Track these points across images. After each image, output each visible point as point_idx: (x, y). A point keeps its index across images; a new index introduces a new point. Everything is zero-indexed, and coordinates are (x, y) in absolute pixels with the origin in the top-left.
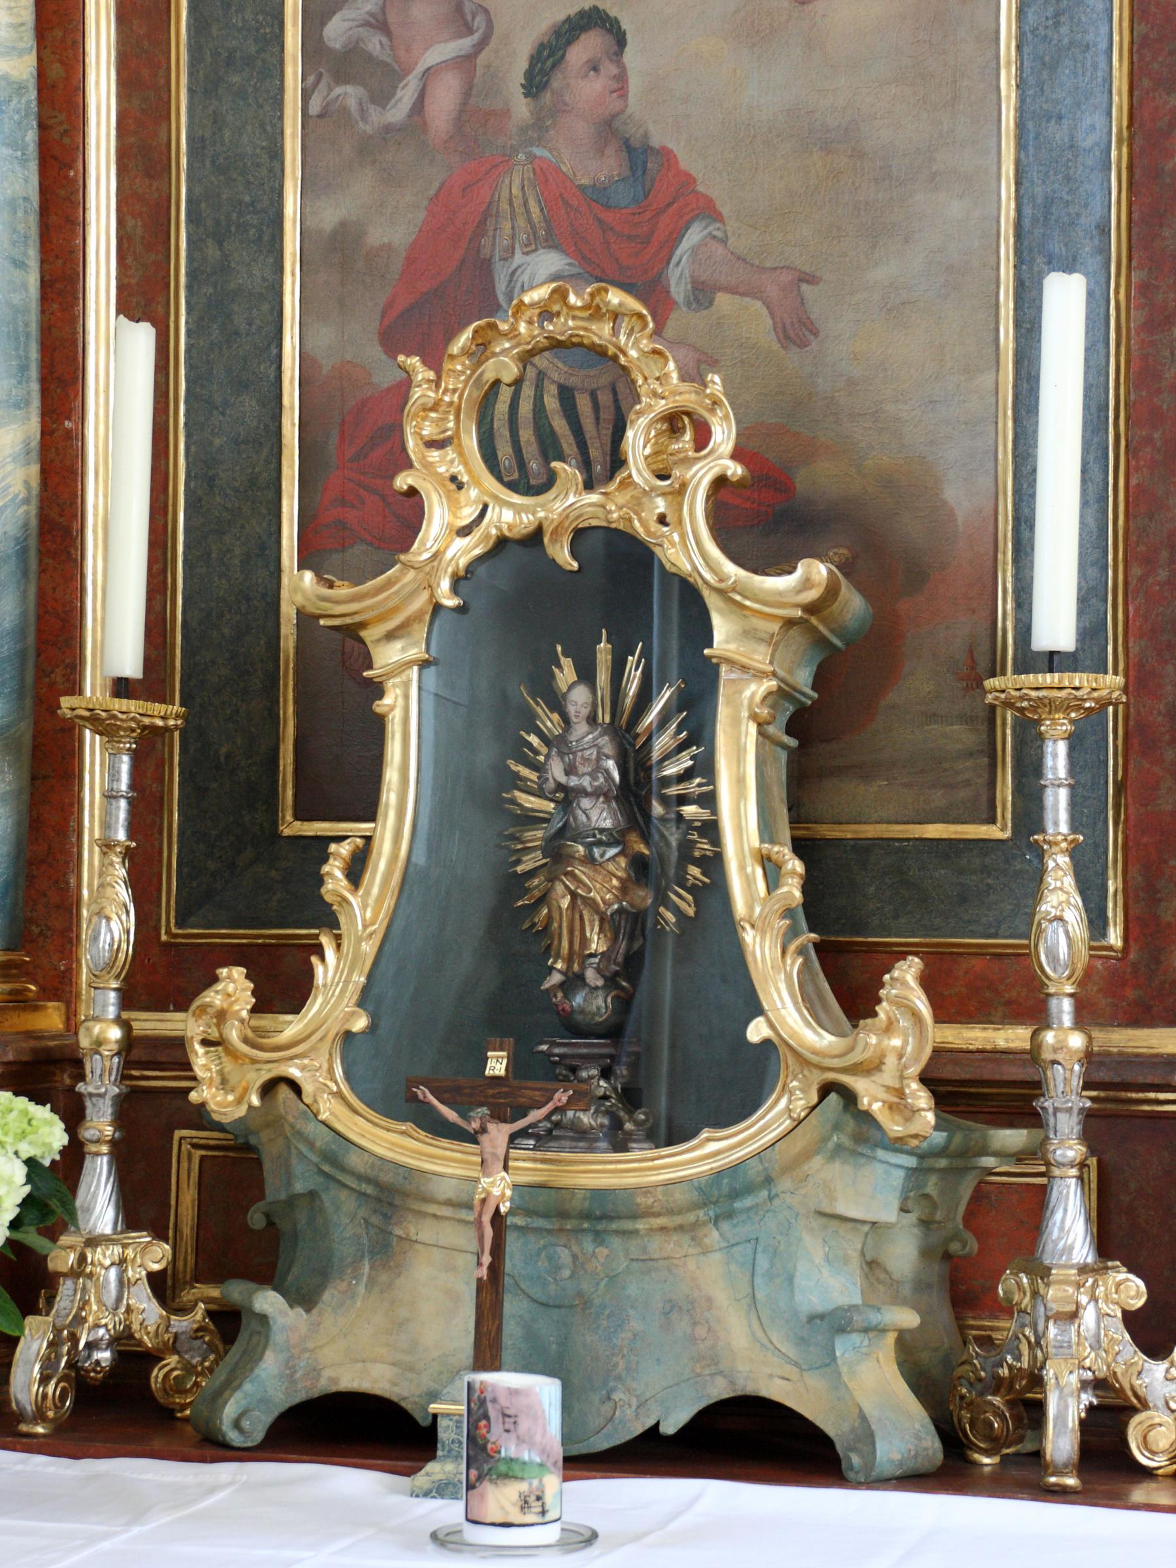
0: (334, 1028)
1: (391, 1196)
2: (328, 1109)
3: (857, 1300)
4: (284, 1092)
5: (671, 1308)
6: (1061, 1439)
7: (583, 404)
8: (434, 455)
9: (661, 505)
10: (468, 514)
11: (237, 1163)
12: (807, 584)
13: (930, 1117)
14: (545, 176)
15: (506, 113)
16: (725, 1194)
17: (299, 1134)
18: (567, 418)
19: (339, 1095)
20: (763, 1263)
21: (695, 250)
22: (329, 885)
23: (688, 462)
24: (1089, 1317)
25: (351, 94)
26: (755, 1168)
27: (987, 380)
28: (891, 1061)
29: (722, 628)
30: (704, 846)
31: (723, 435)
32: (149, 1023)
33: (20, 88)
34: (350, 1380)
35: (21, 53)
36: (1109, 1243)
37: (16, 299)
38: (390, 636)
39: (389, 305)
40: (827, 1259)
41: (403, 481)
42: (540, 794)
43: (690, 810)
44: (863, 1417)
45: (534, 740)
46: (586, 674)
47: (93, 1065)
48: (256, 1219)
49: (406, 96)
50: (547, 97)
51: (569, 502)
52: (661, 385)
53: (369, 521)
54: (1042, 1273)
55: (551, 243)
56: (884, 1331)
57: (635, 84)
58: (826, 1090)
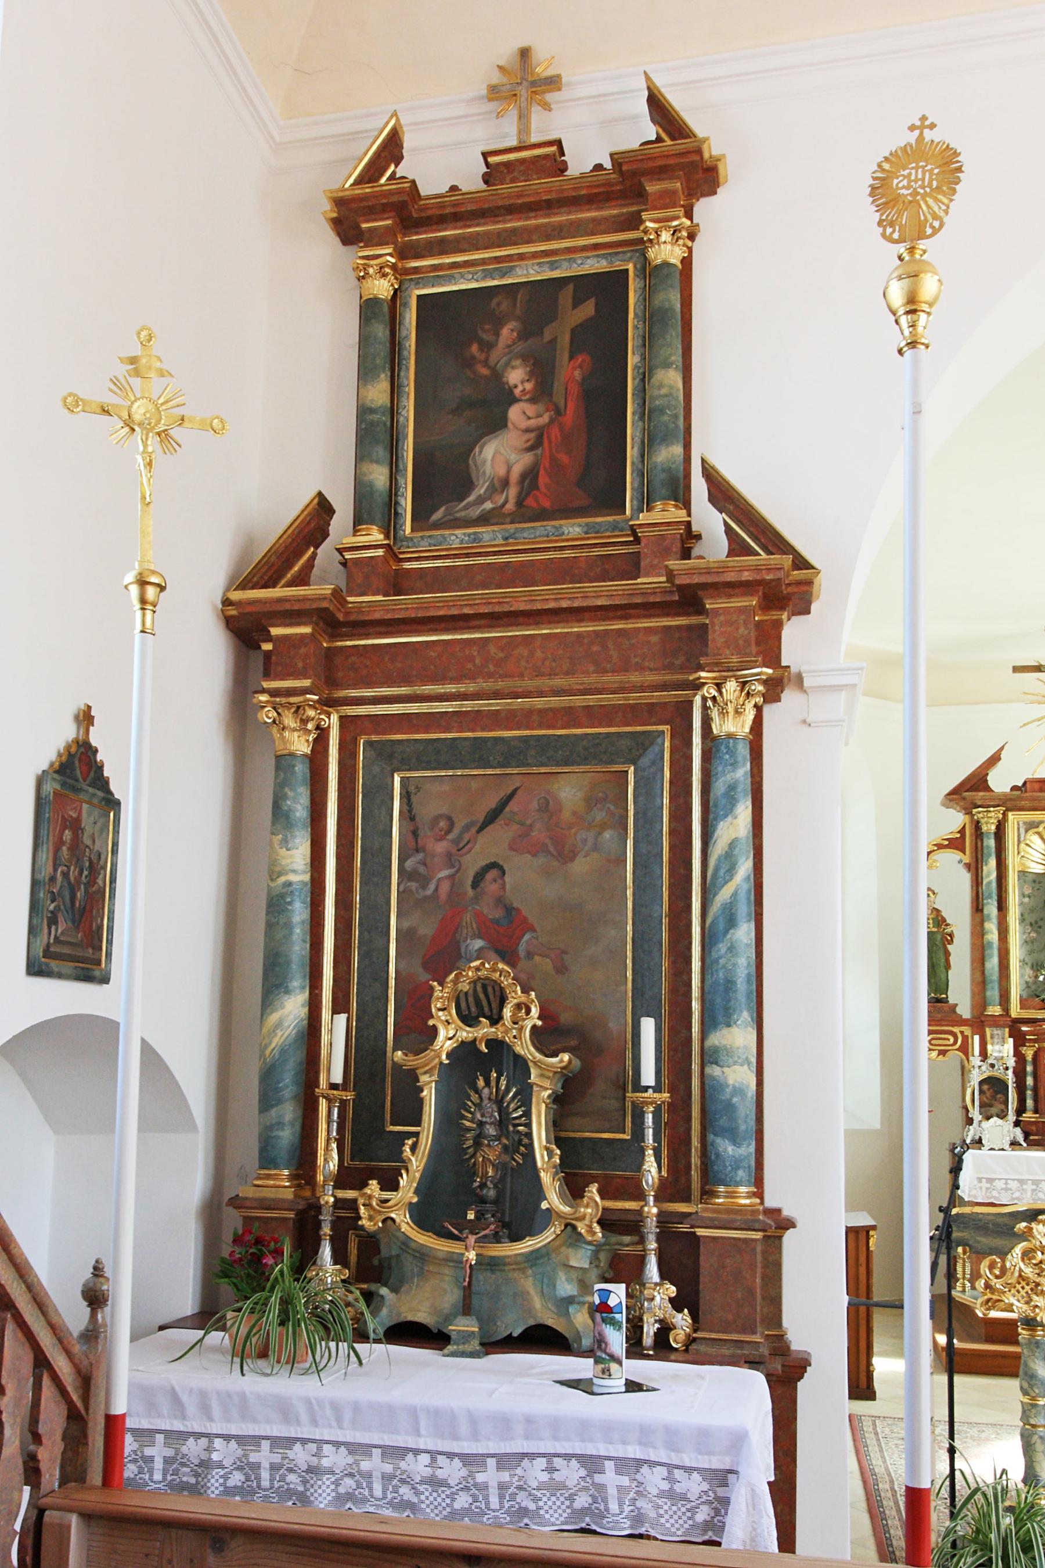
0: (406, 1200)
1: (423, 1255)
2: (404, 1228)
3: (575, 1293)
4: (389, 1222)
5: (515, 1295)
6: (648, 1340)
7: (490, 990)
8: (441, 1013)
9: (514, 1032)
10: (451, 1033)
11: (370, 1243)
12: (562, 1061)
13: (600, 1235)
14: (478, 915)
15: (465, 894)
16: (534, 1258)
17: (394, 1236)
18: (482, 1004)
19: (408, 1223)
20: (546, 1281)
21: (527, 942)
22: (405, 1154)
23: (524, 1020)
24: (658, 1299)
25: (413, 885)
26: (544, 1250)
27: (623, 988)
28: (588, 1217)
29: (534, 1072)
30: (526, 1141)
31: (535, 1011)
32: (342, 1194)
33: (305, 884)
34: (410, 1317)
35: (306, 872)
36: (664, 1275)
37: (303, 953)
38: (425, 1073)
39: (425, 955)
40: (567, 1280)
41: (431, 1023)
42: (472, 1121)
43: (521, 1128)
44: (578, 1332)
45: (469, 1103)
46: (488, 1083)
47: (324, 1211)
48: (376, 1262)
49: (432, 886)
50: (479, 890)
51: (484, 1030)
52: (516, 995)
53: (418, 1032)
54: (643, 1285)
55: (480, 937)
56: (584, 1303)
57: (508, 887)
58: (566, 1225)
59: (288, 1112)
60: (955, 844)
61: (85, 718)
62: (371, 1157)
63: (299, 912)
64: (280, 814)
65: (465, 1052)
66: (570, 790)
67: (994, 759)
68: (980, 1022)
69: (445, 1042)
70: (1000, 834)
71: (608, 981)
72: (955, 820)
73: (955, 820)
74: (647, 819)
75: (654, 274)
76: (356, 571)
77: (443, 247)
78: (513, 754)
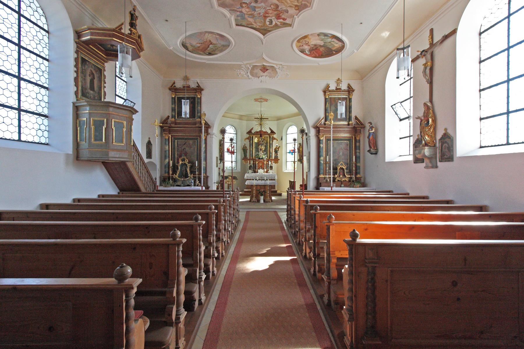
18: (183, 160)
53: (178, 162)
59: (167, 169)
60: (248, 138)
61: (149, 138)
62: (174, 172)
63: (167, 152)
64: (165, 144)
65: (182, 164)
66: (191, 142)
67: (252, 129)
68: (250, 159)
69: (180, 163)
70: (253, 138)
71: (194, 158)
72: (248, 136)
73: (248, 136)
74: (197, 145)
75: (198, 98)
76: (172, 123)
77: (179, 92)
78: (186, 139)
